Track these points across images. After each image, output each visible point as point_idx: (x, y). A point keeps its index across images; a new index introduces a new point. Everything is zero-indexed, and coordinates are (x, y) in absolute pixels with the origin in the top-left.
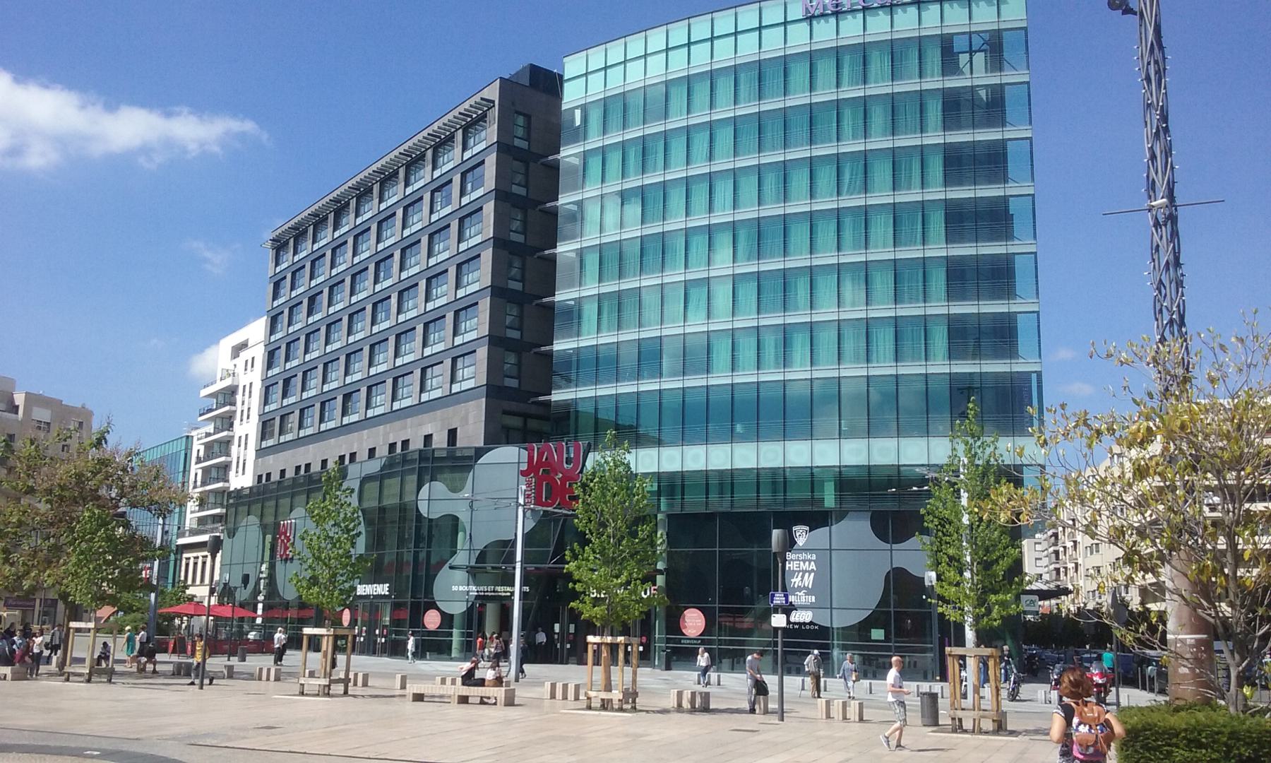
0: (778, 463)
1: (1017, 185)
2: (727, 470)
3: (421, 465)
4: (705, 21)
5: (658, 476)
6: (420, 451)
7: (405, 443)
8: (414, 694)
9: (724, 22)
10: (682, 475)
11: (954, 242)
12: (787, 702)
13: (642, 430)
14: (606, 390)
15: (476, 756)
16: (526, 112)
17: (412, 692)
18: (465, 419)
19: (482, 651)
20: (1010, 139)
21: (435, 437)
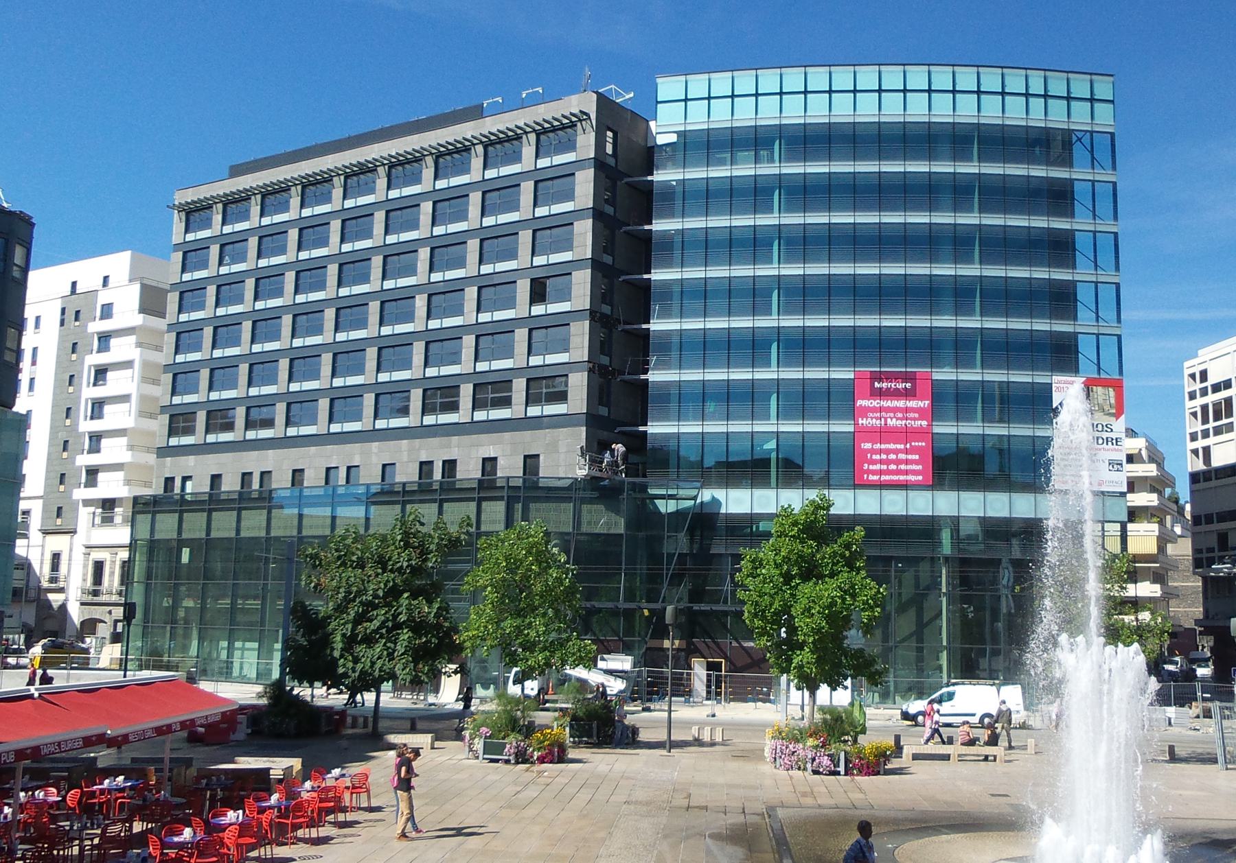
0: (1004, 513)
1: (1104, 273)
2: (902, 515)
3: (480, 495)
4: (922, 71)
5: (984, 521)
6: (480, 481)
7: (450, 466)
8: (913, 754)
9: (793, 78)
10: (1008, 521)
11: (987, 315)
12: (674, 723)
13: (807, 470)
14: (691, 427)
15: (792, 810)
16: (614, 129)
17: (911, 753)
18: (553, 447)
19: (519, 687)
20: (1077, 230)
21: (501, 462)
